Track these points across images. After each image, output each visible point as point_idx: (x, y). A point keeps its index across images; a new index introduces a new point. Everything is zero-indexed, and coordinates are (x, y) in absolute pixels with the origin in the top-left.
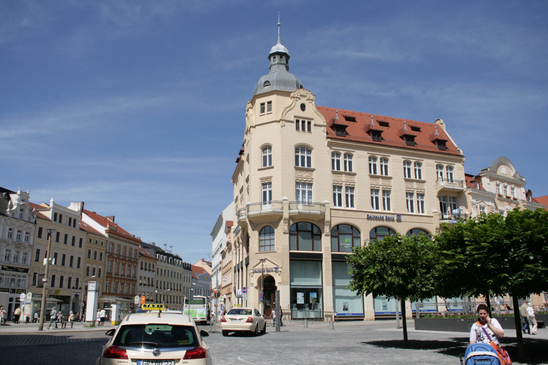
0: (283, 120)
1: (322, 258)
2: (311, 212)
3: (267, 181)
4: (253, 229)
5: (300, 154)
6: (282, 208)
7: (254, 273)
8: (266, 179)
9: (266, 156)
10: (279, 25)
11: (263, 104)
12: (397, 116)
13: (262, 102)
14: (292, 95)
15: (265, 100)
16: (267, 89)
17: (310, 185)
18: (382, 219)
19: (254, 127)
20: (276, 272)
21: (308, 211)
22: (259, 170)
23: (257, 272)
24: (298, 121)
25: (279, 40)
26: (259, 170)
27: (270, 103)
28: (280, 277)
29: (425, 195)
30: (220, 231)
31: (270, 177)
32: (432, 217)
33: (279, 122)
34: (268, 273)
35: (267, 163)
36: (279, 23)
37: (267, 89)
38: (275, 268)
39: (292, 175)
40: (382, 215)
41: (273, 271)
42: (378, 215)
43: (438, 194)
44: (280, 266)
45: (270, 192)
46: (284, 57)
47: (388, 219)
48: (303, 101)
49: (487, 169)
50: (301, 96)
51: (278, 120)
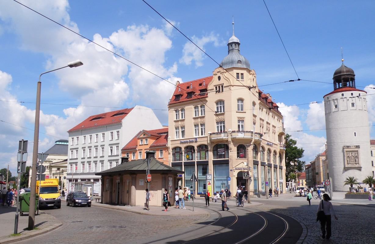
3: (241, 119)
5: (219, 106)
6: (252, 136)
8: (241, 118)
9: (239, 104)
10: (233, 24)
11: (238, 74)
13: (238, 72)
14: (251, 72)
15: (240, 72)
16: (239, 65)
17: (224, 122)
18: (187, 142)
19: (233, 86)
21: (216, 138)
23: (238, 169)
27: (242, 74)
30: (185, 144)
34: (244, 170)
35: (241, 109)
36: (233, 23)
37: (239, 65)
39: (226, 117)
40: (187, 140)
42: (185, 140)
45: (204, 128)
46: (237, 45)
47: (190, 142)
48: (219, 74)
49: (343, 61)
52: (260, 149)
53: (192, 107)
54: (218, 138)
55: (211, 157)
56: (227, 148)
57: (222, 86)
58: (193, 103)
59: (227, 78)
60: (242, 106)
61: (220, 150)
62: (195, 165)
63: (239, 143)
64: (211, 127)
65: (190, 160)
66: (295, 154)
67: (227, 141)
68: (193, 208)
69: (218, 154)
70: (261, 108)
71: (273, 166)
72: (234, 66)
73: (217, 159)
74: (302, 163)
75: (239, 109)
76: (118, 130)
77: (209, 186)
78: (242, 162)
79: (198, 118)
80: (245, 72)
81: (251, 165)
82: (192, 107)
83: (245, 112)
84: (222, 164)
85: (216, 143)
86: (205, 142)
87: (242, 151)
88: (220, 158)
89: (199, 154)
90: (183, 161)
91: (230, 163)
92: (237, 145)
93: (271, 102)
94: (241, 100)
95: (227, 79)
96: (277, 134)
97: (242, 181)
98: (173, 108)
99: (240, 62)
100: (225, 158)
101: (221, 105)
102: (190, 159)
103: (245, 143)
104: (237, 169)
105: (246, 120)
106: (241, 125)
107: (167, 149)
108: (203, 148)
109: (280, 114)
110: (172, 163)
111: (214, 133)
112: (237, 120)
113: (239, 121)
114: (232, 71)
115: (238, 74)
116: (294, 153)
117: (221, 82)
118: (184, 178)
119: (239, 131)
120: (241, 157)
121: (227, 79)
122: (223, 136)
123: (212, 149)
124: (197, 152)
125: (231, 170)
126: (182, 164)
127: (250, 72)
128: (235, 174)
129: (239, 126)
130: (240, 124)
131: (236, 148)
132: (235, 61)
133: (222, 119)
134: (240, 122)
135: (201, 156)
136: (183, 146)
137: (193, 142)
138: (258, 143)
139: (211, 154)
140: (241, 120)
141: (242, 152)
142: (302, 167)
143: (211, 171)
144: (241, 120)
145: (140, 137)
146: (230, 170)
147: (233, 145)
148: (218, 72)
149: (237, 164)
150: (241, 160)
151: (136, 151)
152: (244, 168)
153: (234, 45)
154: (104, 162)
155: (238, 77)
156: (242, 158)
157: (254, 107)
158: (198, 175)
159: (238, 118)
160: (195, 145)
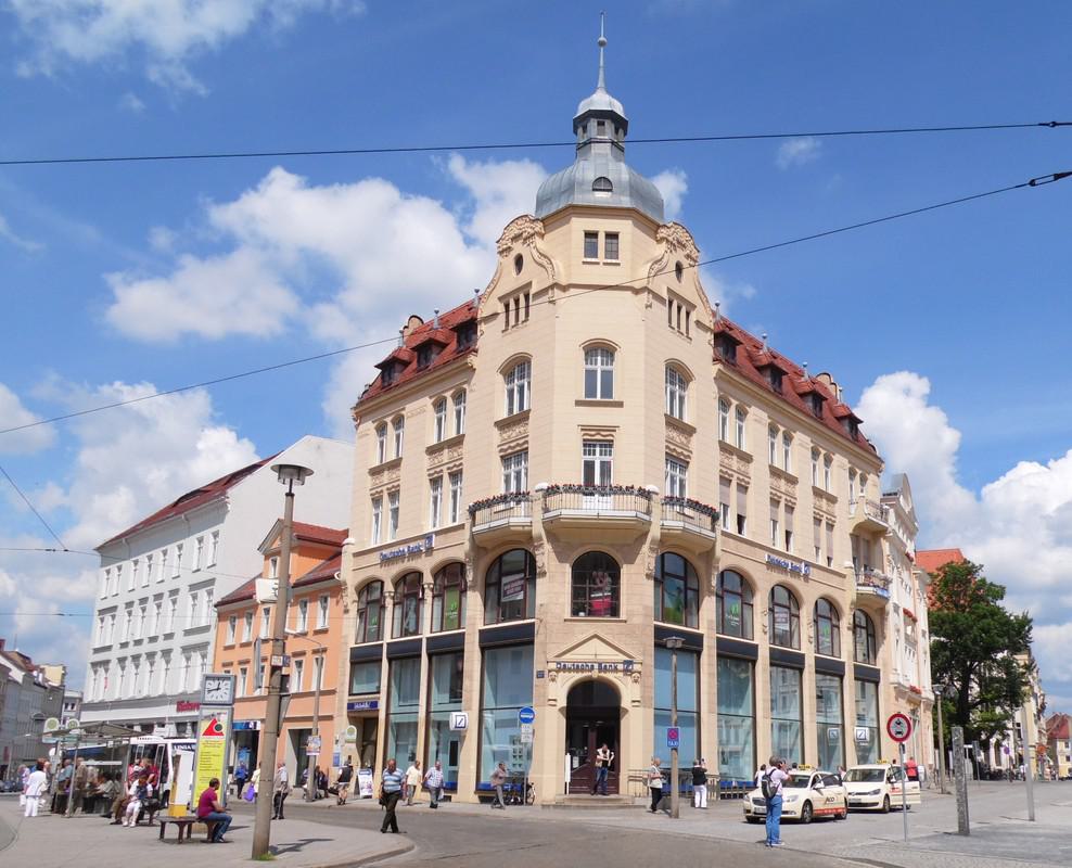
0: (650, 291)
1: (756, 655)
2: (564, 512)
4: (561, 558)
6: (648, 512)
7: (558, 670)
8: (599, 429)
9: (596, 371)
10: (602, 44)
11: (591, 235)
12: (756, 332)
13: (591, 228)
14: (663, 233)
15: (602, 225)
16: (602, 197)
19: (564, 288)
20: (627, 672)
22: (578, 403)
23: (570, 670)
24: (671, 303)
25: (601, 83)
26: (578, 403)
28: (637, 686)
29: (465, 475)
31: (612, 429)
32: (844, 576)
33: (637, 292)
34: (602, 674)
35: (599, 391)
36: (602, 39)
37: (602, 197)
38: (625, 662)
41: (616, 670)
43: (854, 530)
44: (639, 658)
50: (679, 242)
51: (637, 285)
52: (710, 581)
53: (426, 402)
54: (493, 525)
55: (475, 615)
56: (530, 571)
57: (527, 297)
58: (423, 389)
59: (545, 257)
60: (608, 376)
61: (510, 583)
62: (420, 656)
63: (582, 545)
64: (486, 476)
65: (412, 634)
66: (987, 632)
67: (529, 537)
68: (963, 803)
69: (503, 600)
70: (823, 452)
71: (810, 663)
72: (580, 199)
73: (498, 622)
74: (1021, 670)
75: (590, 391)
76: (214, 529)
77: (213, 745)
78: (596, 636)
79: (442, 449)
80: (624, 227)
81: (642, 649)
82: (426, 402)
83: (620, 404)
84: (511, 644)
85: (494, 549)
86: (459, 549)
87: (600, 585)
88: (511, 619)
89: (438, 603)
90: (387, 639)
91: (537, 640)
92: (575, 556)
93: (846, 413)
94: (600, 349)
95: (544, 261)
96: (844, 529)
97: (593, 716)
98: (368, 417)
99: (603, 183)
100: (525, 619)
101: (521, 382)
102: (411, 630)
103: (612, 545)
104: (565, 669)
105: (619, 440)
106: (602, 463)
107: (338, 589)
108: (450, 575)
109: (871, 453)
110: (481, 632)
111: (489, 503)
112: (577, 440)
113: (589, 445)
114: (568, 222)
115: (591, 235)
116: (983, 630)
117: (523, 278)
118: (387, 715)
119: (588, 488)
120: (590, 613)
121: (544, 261)
122: (518, 517)
123: (480, 582)
124: (433, 597)
125: (541, 675)
126: (381, 655)
127: (656, 232)
128: (557, 691)
129: (589, 466)
130: (597, 459)
131: (568, 569)
132: (582, 184)
133: (512, 445)
134: (598, 449)
135: (446, 614)
136: (387, 575)
137: (415, 554)
138: (876, 606)
139: (474, 602)
140: (598, 441)
141: (600, 590)
142: (1026, 684)
143: (471, 679)
144: (598, 441)
145: (274, 547)
146: (535, 674)
147: (553, 555)
148: (515, 238)
149: (568, 644)
150: (586, 627)
151: (256, 606)
152: (600, 664)
153: (593, 124)
154: (172, 655)
155: (591, 251)
156: (600, 615)
157: (741, 420)
158: (433, 702)
159: (585, 428)
160: (426, 565)
